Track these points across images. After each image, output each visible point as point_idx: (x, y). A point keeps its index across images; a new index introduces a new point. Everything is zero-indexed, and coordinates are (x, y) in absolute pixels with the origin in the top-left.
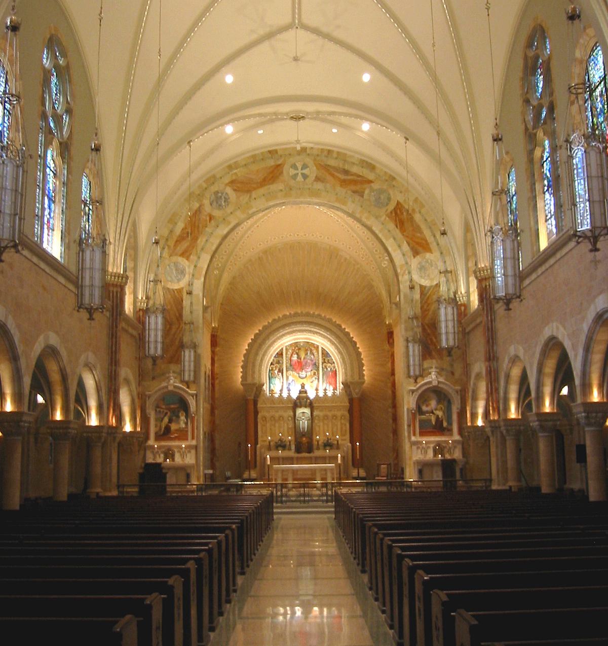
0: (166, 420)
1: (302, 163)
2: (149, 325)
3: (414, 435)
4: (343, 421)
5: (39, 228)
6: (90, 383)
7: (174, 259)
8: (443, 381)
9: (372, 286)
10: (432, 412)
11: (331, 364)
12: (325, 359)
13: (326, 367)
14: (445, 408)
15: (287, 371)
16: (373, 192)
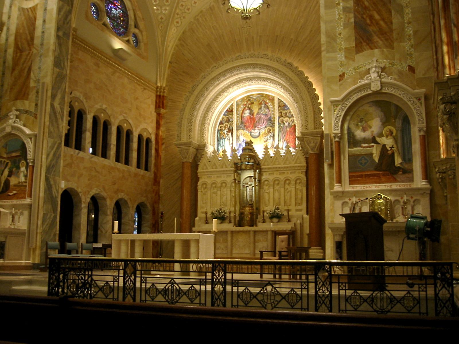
3: (340, 181)
4: (298, 186)
8: (393, 81)
11: (290, 118)
12: (281, 113)
13: (283, 122)
14: (397, 131)
15: (237, 130)
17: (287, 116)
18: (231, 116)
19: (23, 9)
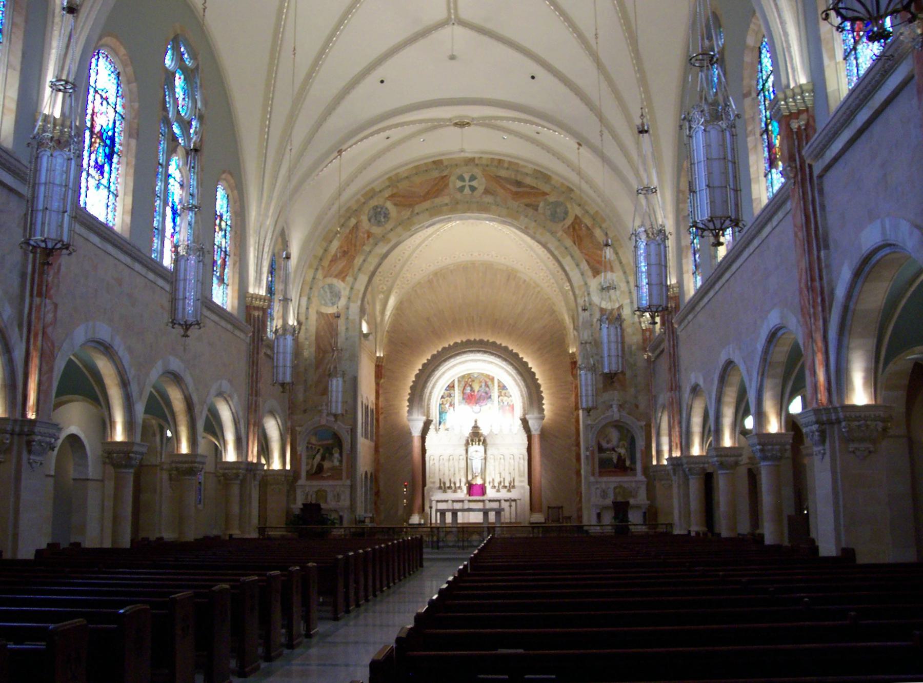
0: (318, 457)
1: (470, 174)
2: (277, 349)
5: (159, 243)
6: (226, 414)
7: (329, 280)
9: (553, 312)
10: (613, 449)
13: (502, 400)
16: (548, 205)
17: (506, 396)
18: (452, 391)
19: (322, 314)
